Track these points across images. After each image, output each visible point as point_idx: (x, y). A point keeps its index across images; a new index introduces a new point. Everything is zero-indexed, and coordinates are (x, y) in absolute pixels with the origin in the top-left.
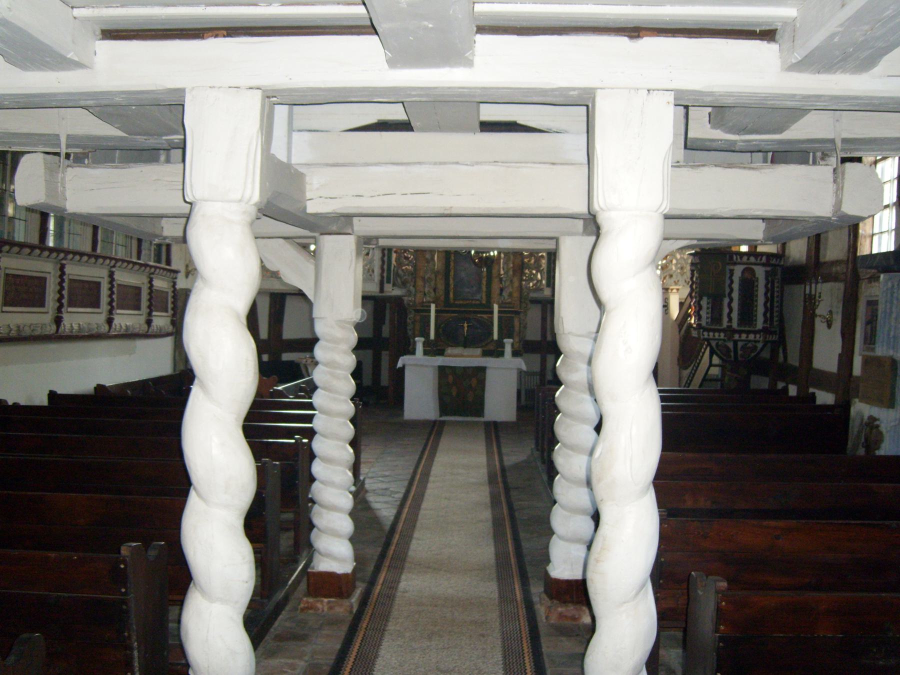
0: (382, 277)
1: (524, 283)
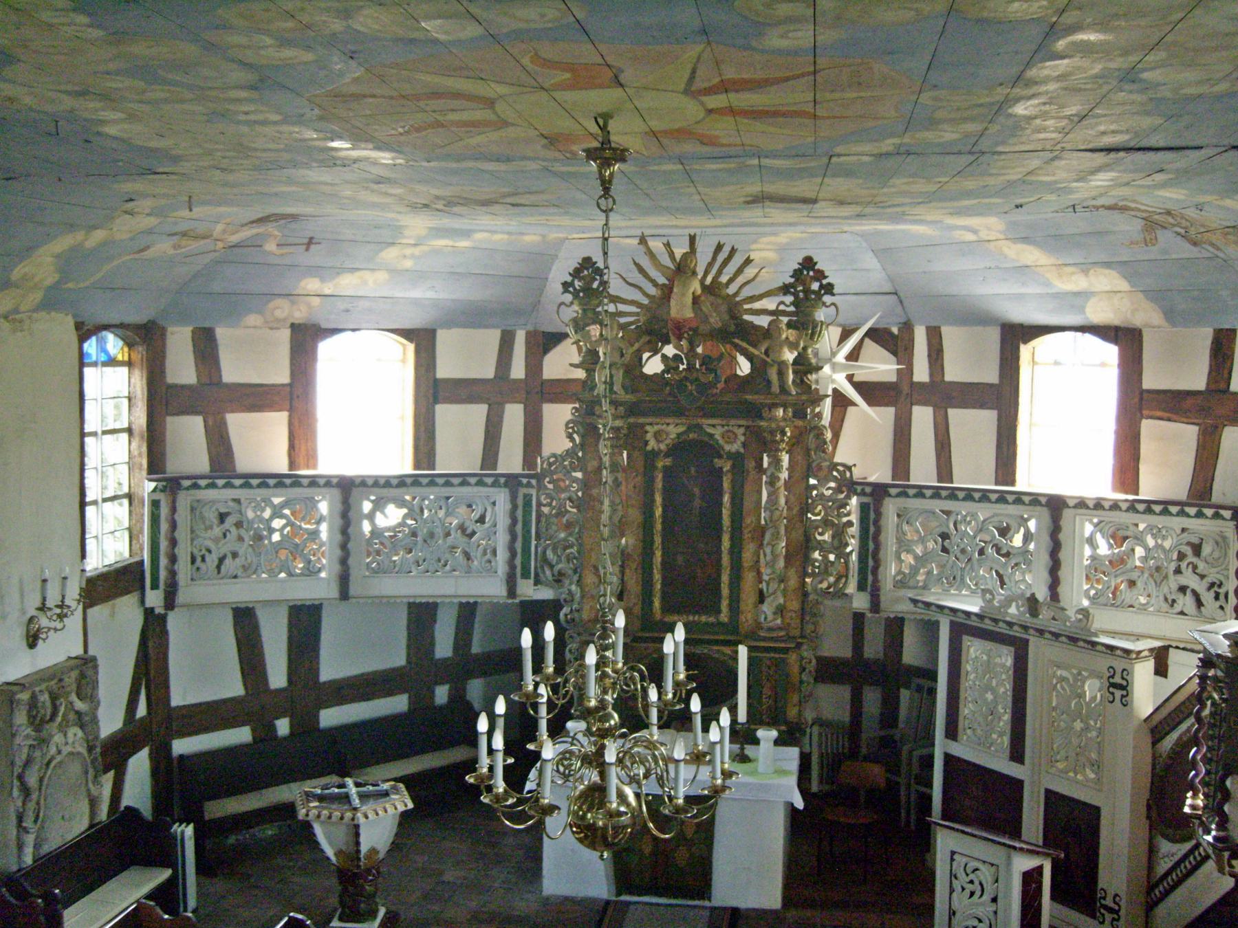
0: (512, 566)
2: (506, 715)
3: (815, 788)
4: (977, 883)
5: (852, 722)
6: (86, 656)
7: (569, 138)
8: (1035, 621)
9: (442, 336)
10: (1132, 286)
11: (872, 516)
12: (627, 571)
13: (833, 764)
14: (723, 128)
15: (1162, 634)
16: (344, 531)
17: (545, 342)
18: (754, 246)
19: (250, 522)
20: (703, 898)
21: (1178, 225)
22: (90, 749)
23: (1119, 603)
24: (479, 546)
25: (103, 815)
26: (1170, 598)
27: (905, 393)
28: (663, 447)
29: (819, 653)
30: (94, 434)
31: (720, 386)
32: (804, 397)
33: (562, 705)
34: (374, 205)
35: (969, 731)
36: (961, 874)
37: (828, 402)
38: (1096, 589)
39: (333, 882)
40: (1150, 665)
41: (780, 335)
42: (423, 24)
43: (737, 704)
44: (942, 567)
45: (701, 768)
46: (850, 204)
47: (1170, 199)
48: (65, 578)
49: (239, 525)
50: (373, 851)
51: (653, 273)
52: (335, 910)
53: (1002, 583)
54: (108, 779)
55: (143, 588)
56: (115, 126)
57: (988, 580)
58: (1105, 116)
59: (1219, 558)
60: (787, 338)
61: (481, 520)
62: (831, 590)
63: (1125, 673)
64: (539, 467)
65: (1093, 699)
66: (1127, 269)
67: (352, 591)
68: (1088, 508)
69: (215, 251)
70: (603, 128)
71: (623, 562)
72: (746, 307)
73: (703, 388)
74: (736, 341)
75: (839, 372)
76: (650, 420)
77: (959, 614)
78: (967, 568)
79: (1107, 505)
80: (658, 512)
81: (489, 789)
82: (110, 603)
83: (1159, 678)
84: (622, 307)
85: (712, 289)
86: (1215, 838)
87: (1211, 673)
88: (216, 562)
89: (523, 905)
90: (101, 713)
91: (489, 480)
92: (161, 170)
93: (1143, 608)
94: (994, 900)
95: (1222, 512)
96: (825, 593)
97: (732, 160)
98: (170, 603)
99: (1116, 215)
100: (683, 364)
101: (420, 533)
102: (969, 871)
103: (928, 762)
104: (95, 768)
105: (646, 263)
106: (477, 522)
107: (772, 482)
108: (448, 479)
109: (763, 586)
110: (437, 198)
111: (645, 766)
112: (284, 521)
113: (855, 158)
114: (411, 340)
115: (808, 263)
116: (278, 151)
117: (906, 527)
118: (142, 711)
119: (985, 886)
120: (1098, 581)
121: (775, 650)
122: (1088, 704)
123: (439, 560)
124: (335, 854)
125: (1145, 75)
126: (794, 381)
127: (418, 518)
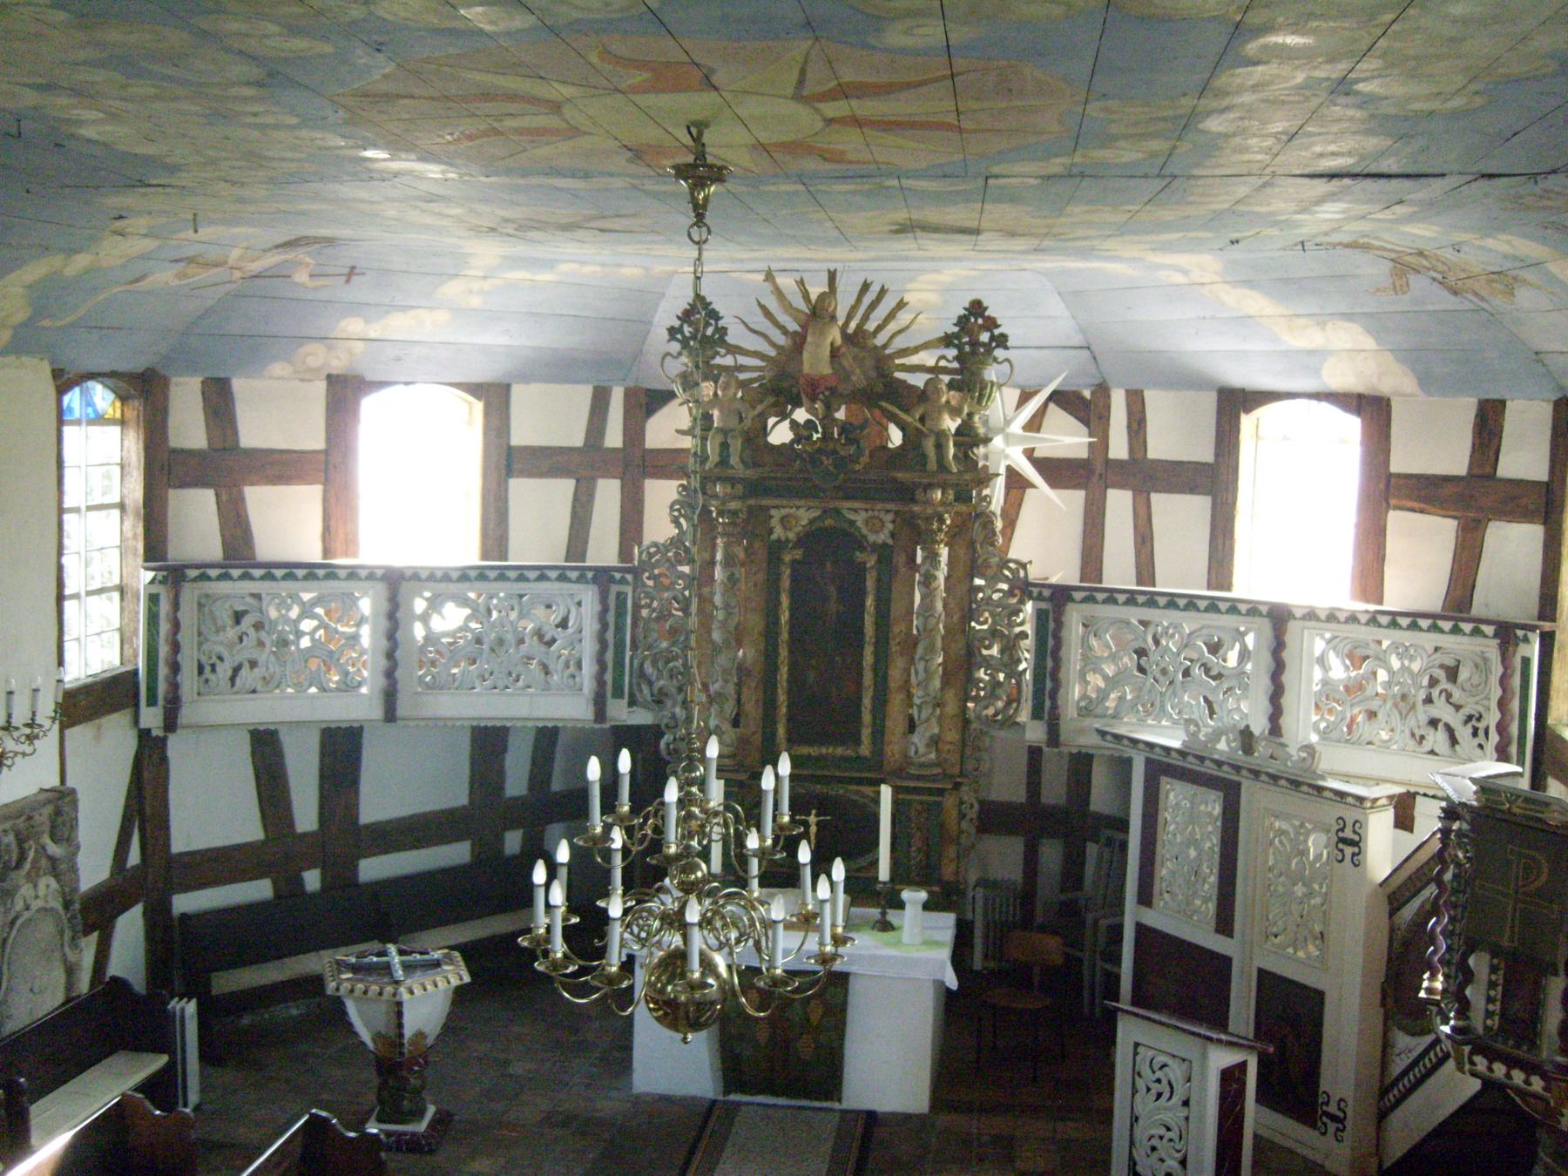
0: (601, 683)
1: (970, 705)
2: (570, 865)
3: (978, 963)
4: (1165, 1082)
5: (1025, 884)
6: (62, 788)
7: (659, 150)
8: (1249, 759)
9: (518, 392)
10: (1379, 344)
11: (1052, 625)
12: (745, 690)
13: (999, 934)
14: (849, 141)
15: (1407, 778)
16: (391, 636)
17: (647, 402)
18: (909, 286)
19: (274, 623)
20: (828, 1098)
21: (1434, 269)
22: (67, 905)
23: (1355, 739)
24: (559, 657)
25: (84, 985)
26: (1418, 733)
27: (1098, 472)
28: (791, 535)
29: (983, 795)
30: (77, 510)
31: (865, 459)
32: (967, 477)
33: (638, 852)
34: (427, 227)
35: (1166, 896)
36: (1146, 1071)
37: (1000, 483)
38: (1327, 721)
39: (371, 1076)
40: (1389, 815)
41: (940, 398)
42: (462, 12)
43: (877, 860)
44: (1138, 690)
45: (811, 934)
46: (1021, 235)
47: (1421, 237)
48: (36, 690)
49: (258, 626)
50: (420, 1035)
51: (784, 319)
52: (372, 1110)
53: (1212, 712)
54: (90, 944)
55: (137, 705)
56: (92, 126)
57: (1195, 709)
58: (1320, 134)
59: (1479, 685)
60: (948, 402)
61: (563, 624)
62: (999, 717)
63: (1357, 825)
64: (636, 557)
65: (1318, 857)
66: (1374, 323)
67: (401, 711)
68: (1318, 619)
69: (230, 282)
70: (697, 140)
71: (740, 679)
72: (897, 361)
73: (842, 463)
74: (884, 404)
75: (1014, 445)
76: (776, 502)
77: (1157, 749)
78: (1168, 693)
79: (1342, 617)
80: (785, 617)
81: (546, 953)
82: (97, 721)
83: (1401, 832)
84: (743, 360)
85: (856, 339)
86: (1453, 1029)
87: (1455, 826)
88: (229, 673)
89: (608, 1105)
90: (81, 859)
91: (574, 575)
92: (155, 182)
93: (1385, 745)
94: (1186, 1103)
95: (1484, 628)
96: (991, 721)
97: (865, 180)
98: (171, 724)
99: (1357, 255)
100: (817, 432)
101: (486, 640)
102: (1156, 1067)
103: (1116, 933)
104: (73, 927)
105: (773, 305)
106: (557, 626)
107: (928, 580)
108: (522, 573)
109: (915, 711)
110: (507, 220)
111: (738, 928)
112: (315, 623)
113: (1018, 180)
114: (478, 398)
115: (977, 308)
116: (300, 160)
117: (1094, 642)
118: (134, 857)
119: (1174, 1085)
120: (1330, 711)
121: (930, 791)
122: (1312, 864)
123: (510, 674)
124: (373, 1040)
125: (1360, 87)
126: (955, 456)
127: (485, 620)
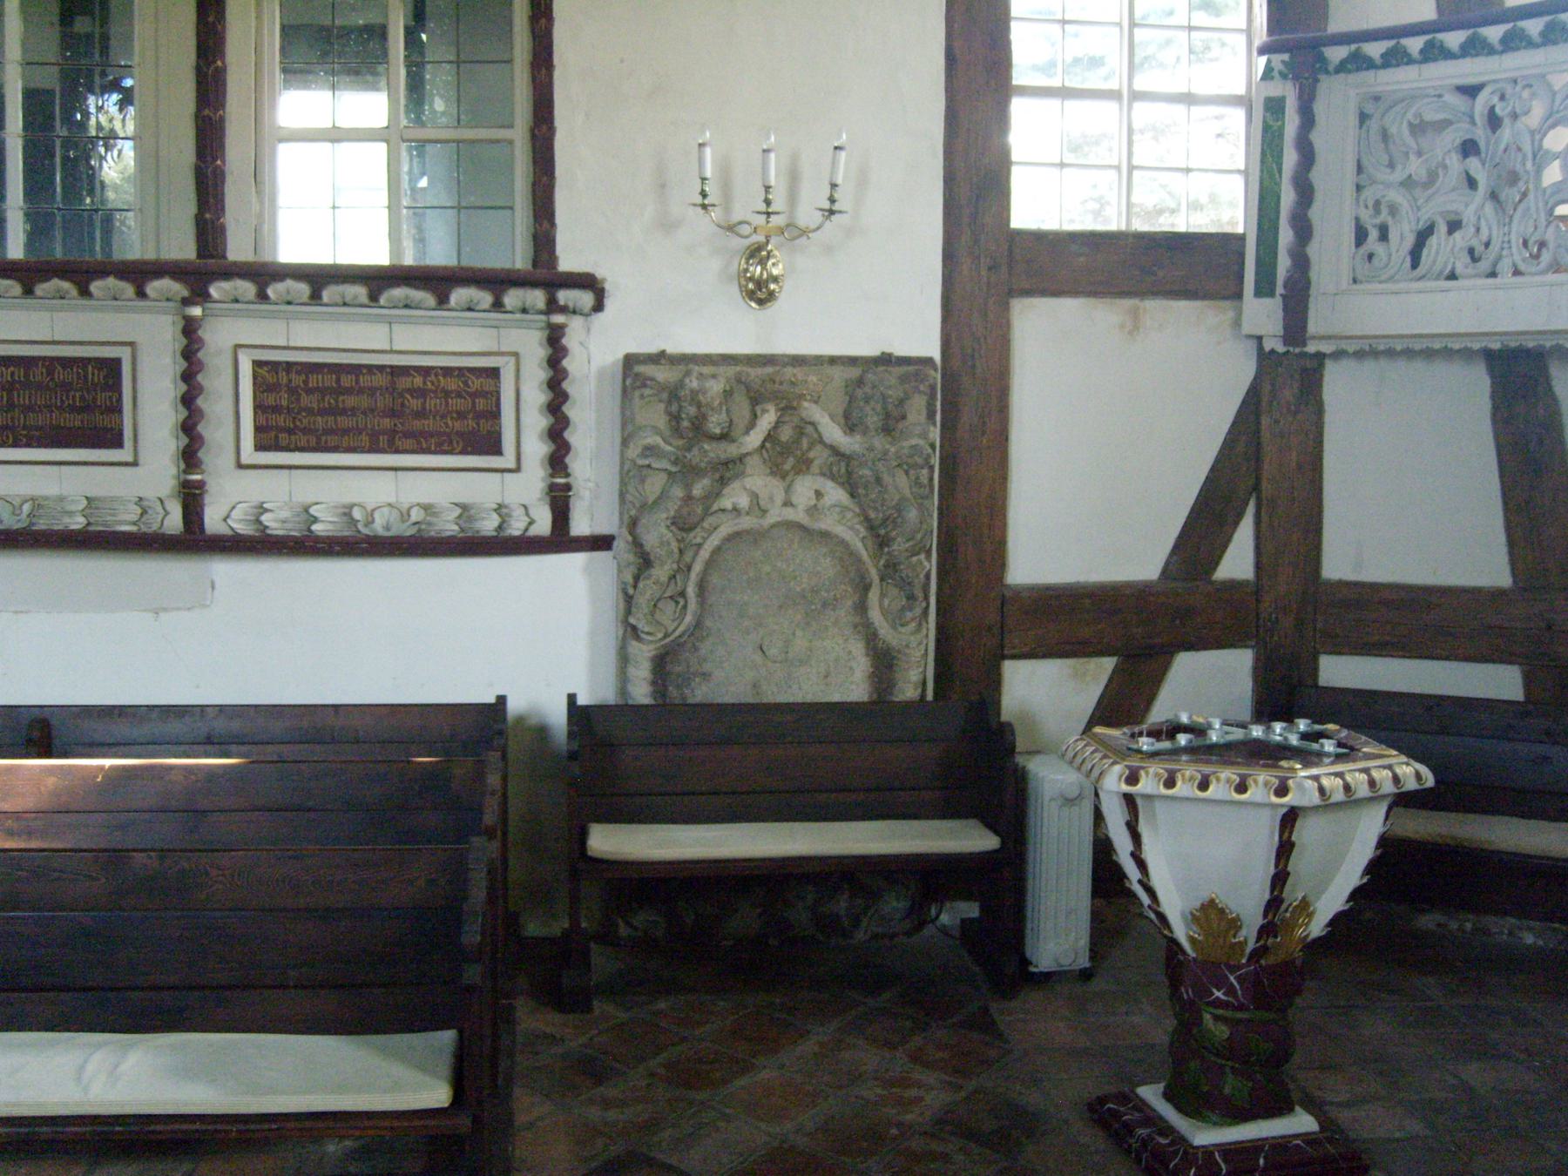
55: (1239, 295)
88: (1410, 240)
